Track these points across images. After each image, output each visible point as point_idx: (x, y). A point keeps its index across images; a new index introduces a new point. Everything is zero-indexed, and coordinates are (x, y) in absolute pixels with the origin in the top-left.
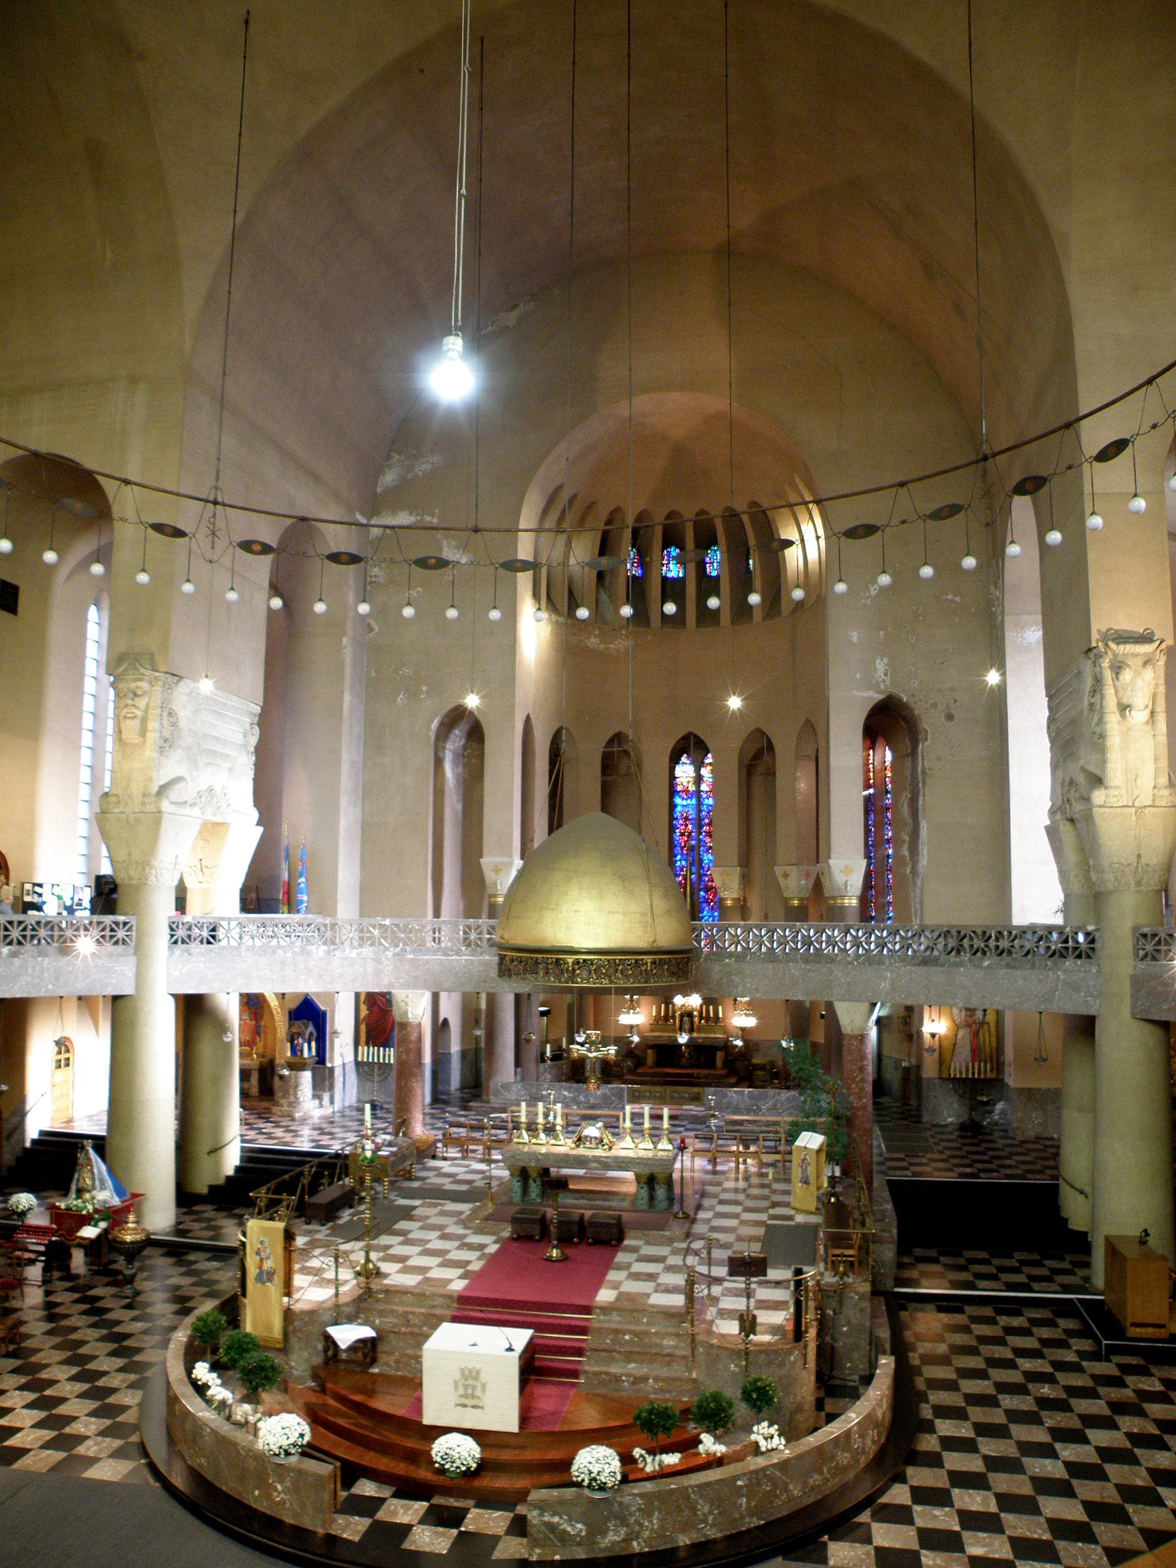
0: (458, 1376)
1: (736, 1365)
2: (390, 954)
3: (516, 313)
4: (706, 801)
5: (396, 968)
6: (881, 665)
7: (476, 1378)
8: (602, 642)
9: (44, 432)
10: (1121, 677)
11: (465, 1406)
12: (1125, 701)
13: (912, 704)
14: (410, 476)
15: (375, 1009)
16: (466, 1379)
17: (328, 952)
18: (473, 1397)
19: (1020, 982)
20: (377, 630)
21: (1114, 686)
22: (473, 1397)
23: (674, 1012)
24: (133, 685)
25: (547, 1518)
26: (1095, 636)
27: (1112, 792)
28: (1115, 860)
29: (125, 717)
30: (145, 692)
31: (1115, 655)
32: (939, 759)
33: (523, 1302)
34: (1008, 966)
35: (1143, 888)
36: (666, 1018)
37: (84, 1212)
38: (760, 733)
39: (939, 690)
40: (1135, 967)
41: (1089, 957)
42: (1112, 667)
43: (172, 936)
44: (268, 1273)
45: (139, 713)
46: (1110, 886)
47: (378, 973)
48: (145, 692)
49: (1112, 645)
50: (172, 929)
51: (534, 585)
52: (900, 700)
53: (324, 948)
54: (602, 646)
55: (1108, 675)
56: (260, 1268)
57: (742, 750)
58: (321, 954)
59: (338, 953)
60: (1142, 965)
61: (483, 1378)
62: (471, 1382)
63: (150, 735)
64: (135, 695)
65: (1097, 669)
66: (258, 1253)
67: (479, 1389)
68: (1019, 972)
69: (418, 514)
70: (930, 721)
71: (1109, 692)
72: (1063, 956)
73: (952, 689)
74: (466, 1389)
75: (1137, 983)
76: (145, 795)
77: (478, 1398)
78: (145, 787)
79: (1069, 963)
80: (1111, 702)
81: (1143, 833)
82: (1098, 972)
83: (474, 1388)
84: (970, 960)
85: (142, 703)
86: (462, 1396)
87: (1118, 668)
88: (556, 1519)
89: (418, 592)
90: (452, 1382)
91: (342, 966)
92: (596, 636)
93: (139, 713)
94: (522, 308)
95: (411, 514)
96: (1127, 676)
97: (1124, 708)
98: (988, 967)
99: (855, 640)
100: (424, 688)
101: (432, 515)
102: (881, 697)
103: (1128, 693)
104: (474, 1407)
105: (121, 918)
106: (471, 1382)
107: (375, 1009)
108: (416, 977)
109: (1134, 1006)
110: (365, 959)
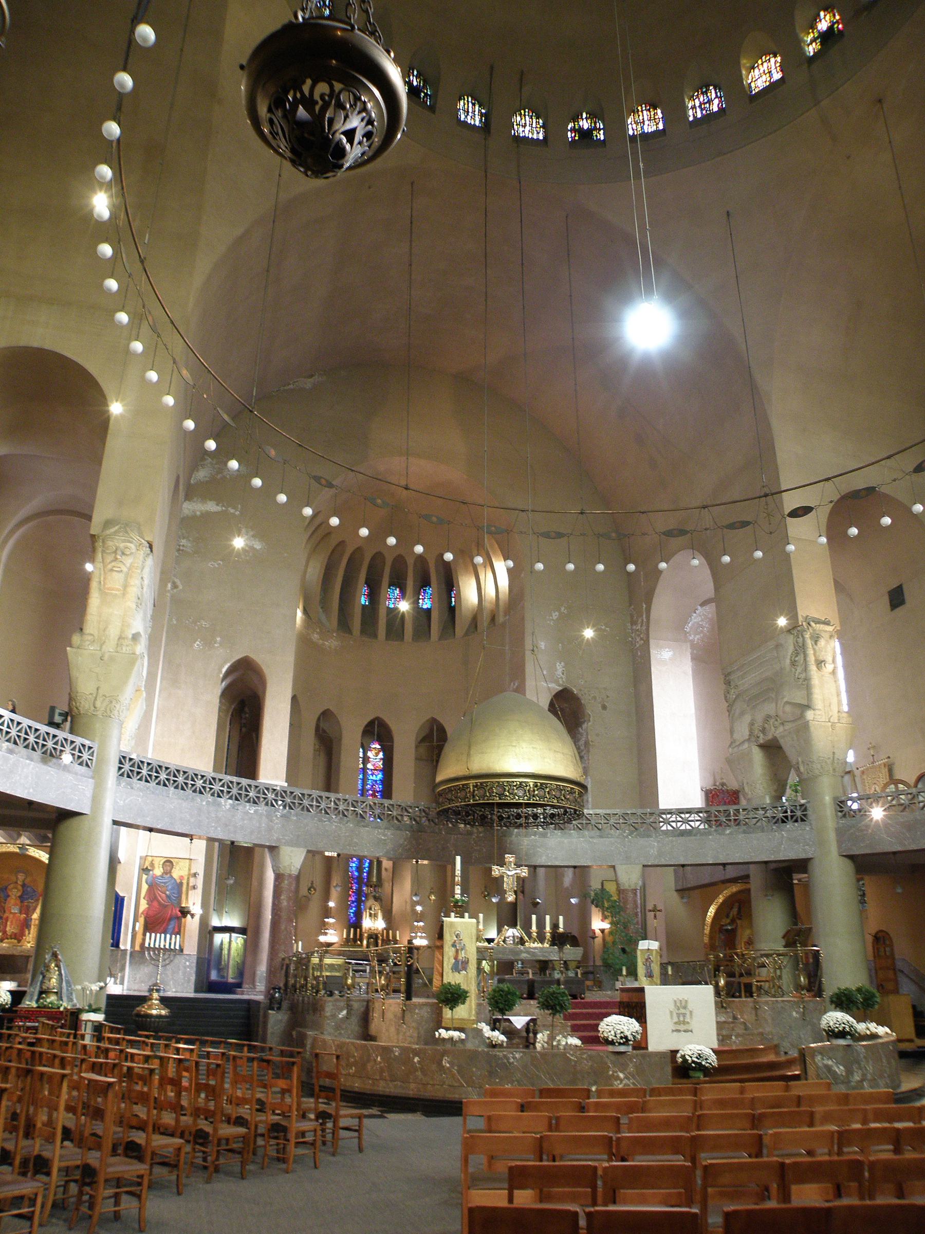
0: (672, 1007)
1: (797, 1012)
2: (279, 814)
3: (311, 380)
4: (371, 777)
5: (283, 826)
6: (560, 667)
7: (685, 1008)
9: (43, 332)
10: (819, 643)
11: (678, 1031)
12: (821, 658)
13: (580, 696)
14: (219, 476)
15: (155, 904)
16: (678, 1009)
17: (233, 806)
18: (684, 1023)
19: (755, 842)
20: (181, 587)
21: (814, 649)
22: (684, 1023)
23: (361, 935)
24: (122, 545)
25: (825, 1062)
26: (800, 619)
27: (818, 712)
28: (821, 754)
29: (112, 570)
30: (132, 553)
31: (814, 630)
32: (597, 735)
33: (600, 1002)
34: (744, 832)
35: (837, 774)
36: (355, 940)
37: (62, 1009)
38: (433, 721)
39: (597, 688)
40: (838, 823)
41: (803, 820)
42: (812, 637)
43: (120, 768)
44: (462, 962)
45: (125, 569)
46: (817, 772)
47: (270, 829)
48: (132, 553)
49: (812, 624)
50: (121, 763)
51: (325, 574)
52: (572, 693)
53: (230, 801)
55: (809, 642)
56: (456, 958)
57: (417, 734)
58: (228, 807)
59: (240, 808)
60: (843, 821)
61: (690, 1006)
62: (682, 1011)
63: (130, 590)
64: (123, 554)
65: (800, 640)
66: (454, 945)
67: (688, 1016)
68: (753, 835)
69: (223, 506)
70: (591, 708)
71: (810, 652)
72: (783, 822)
73: (605, 689)
74: (678, 1017)
75: (840, 832)
76: (120, 638)
77: (688, 1023)
78: (122, 631)
79: (789, 825)
80: (811, 659)
81: (836, 739)
82: (812, 828)
83: (684, 1015)
84: (715, 831)
85: (128, 561)
86: (676, 1023)
87: (816, 639)
88: (830, 1063)
89: (219, 564)
90: (668, 1012)
91: (243, 819)
92: (317, 633)
93: (125, 569)
94: (316, 378)
95: (217, 505)
96: (822, 642)
97: (820, 663)
98: (731, 833)
99: (543, 647)
100: (218, 639)
101: (235, 508)
102: (560, 688)
103: (823, 653)
104: (685, 1031)
105: (87, 743)
106: (682, 1011)
107: (155, 904)
108: (298, 836)
109: (839, 847)
110: (261, 814)
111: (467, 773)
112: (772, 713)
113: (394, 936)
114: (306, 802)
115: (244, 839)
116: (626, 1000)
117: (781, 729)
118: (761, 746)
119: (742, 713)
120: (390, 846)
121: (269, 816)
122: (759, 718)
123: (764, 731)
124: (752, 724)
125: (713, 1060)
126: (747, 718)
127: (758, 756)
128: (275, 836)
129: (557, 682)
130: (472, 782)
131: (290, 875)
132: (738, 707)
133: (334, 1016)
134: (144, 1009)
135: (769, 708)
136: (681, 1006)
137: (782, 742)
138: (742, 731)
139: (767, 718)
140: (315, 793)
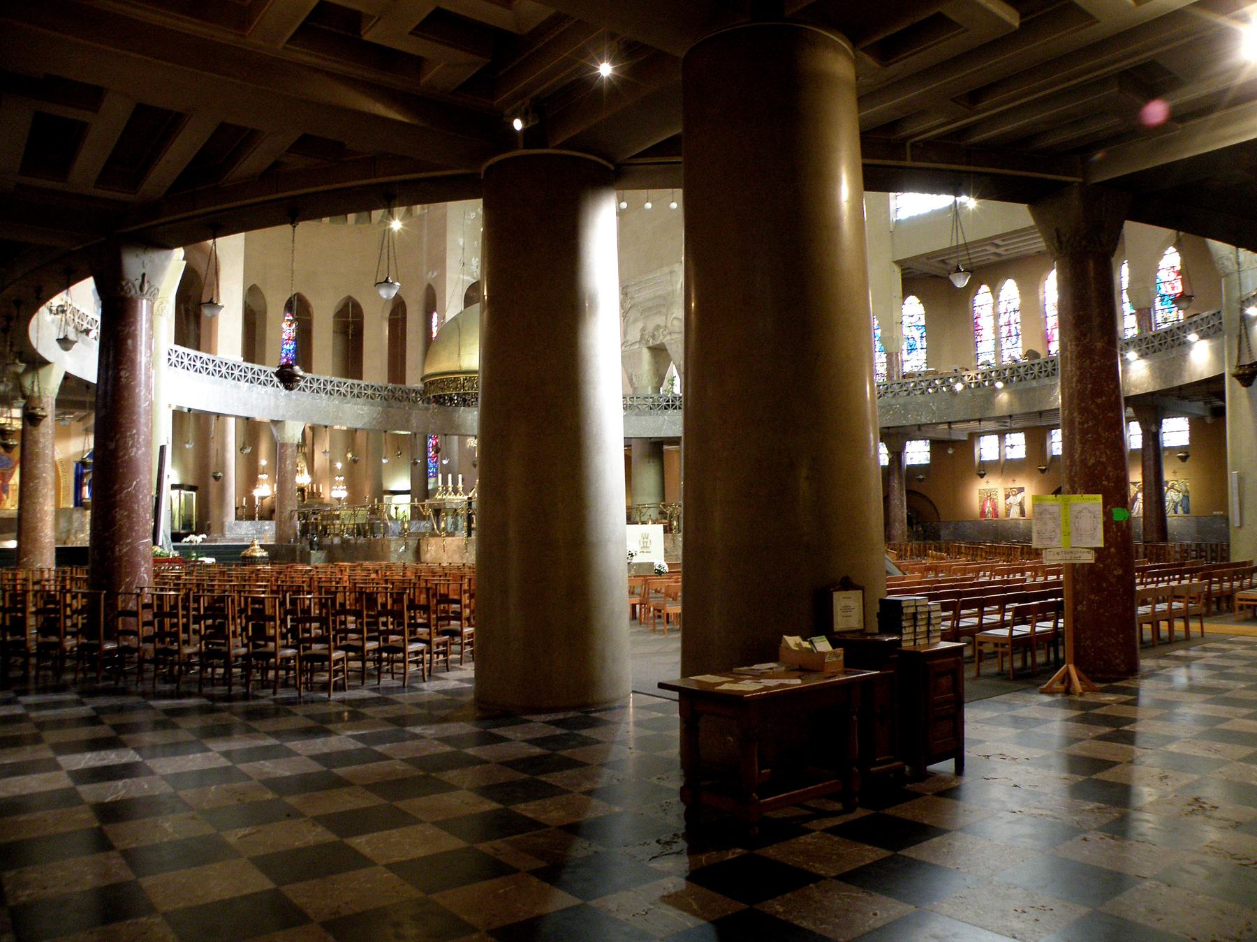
17: (249, 388)
38: (349, 298)
47: (277, 407)
79: (670, 411)
111: (458, 369)
112: (663, 324)
113: (318, 489)
114: (315, 386)
115: (258, 416)
116: (1134, 523)
117: (668, 337)
118: (649, 348)
119: (635, 321)
120: (366, 419)
121: (276, 397)
122: (650, 327)
123: (653, 336)
124: (643, 329)
125: (667, 569)
126: (640, 325)
127: (646, 355)
128: (281, 412)
129: (471, 275)
130: (462, 377)
131: (292, 445)
132: (632, 316)
133: (396, 551)
134: (248, 553)
135: (660, 320)
136: (645, 537)
137: (668, 347)
138: (635, 334)
139: (658, 327)
140: (336, 380)
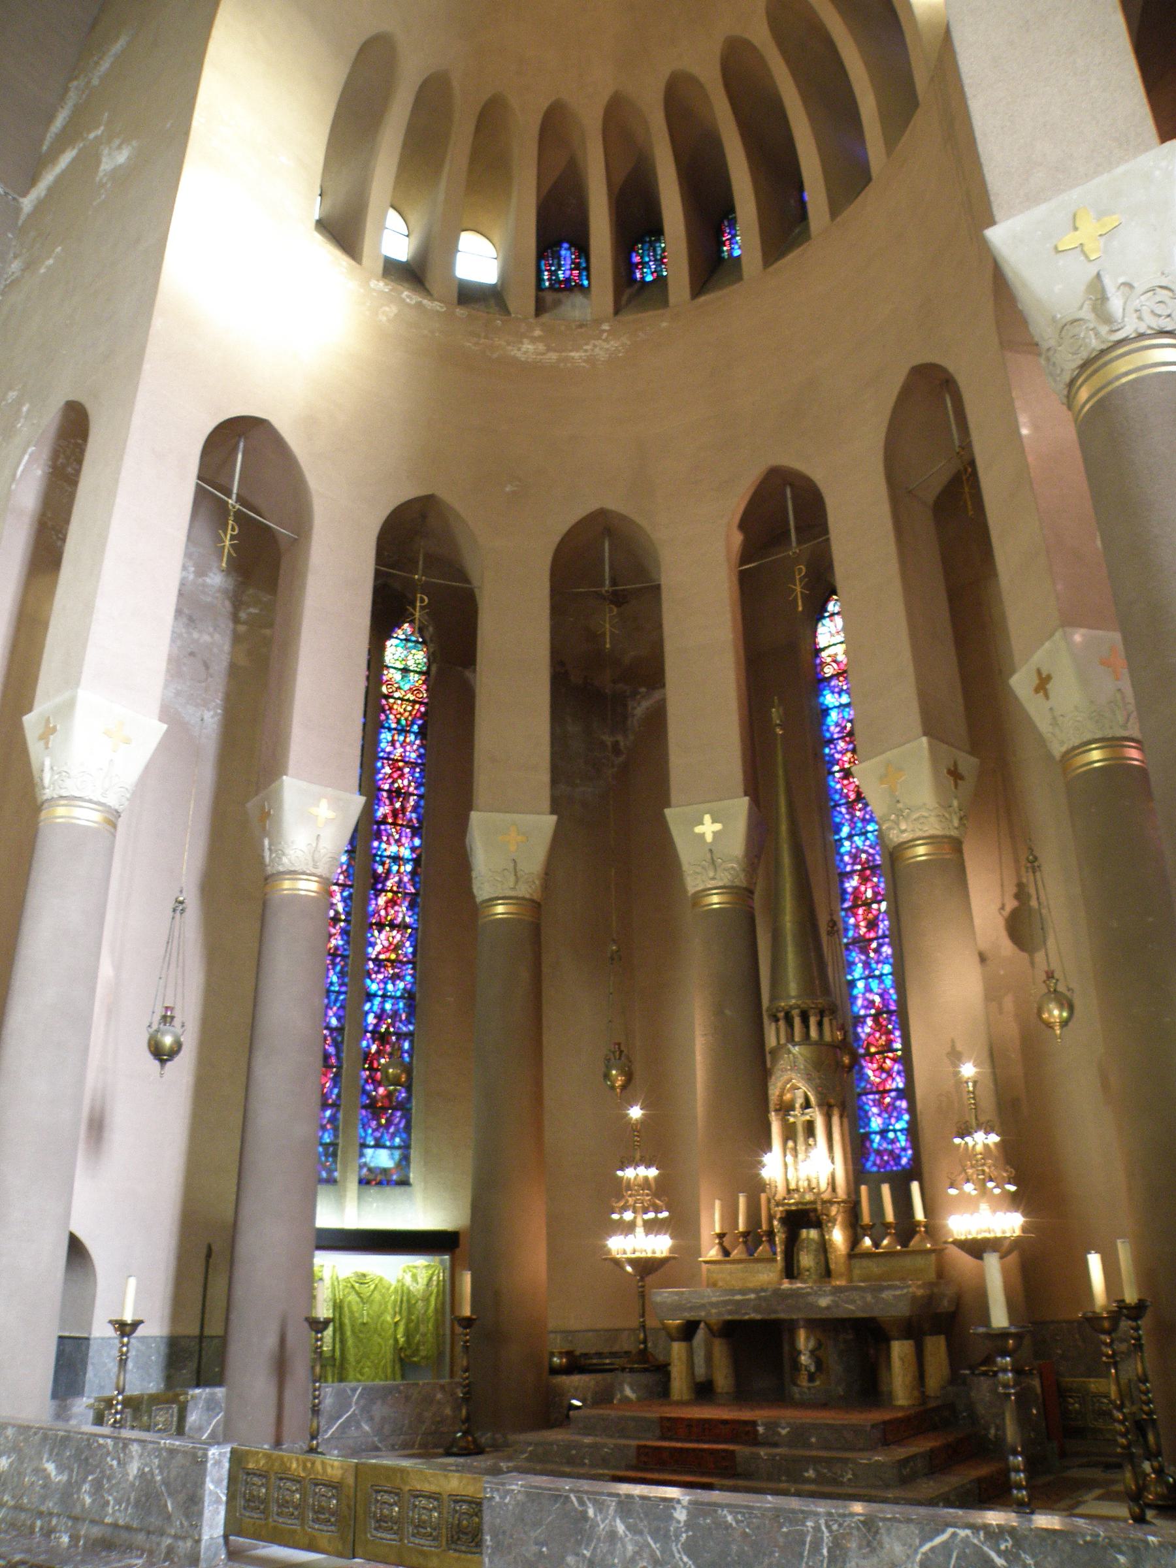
8: (549, 349)
54: (553, 356)
92: (534, 340)
